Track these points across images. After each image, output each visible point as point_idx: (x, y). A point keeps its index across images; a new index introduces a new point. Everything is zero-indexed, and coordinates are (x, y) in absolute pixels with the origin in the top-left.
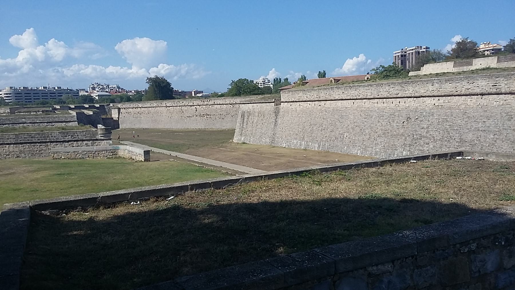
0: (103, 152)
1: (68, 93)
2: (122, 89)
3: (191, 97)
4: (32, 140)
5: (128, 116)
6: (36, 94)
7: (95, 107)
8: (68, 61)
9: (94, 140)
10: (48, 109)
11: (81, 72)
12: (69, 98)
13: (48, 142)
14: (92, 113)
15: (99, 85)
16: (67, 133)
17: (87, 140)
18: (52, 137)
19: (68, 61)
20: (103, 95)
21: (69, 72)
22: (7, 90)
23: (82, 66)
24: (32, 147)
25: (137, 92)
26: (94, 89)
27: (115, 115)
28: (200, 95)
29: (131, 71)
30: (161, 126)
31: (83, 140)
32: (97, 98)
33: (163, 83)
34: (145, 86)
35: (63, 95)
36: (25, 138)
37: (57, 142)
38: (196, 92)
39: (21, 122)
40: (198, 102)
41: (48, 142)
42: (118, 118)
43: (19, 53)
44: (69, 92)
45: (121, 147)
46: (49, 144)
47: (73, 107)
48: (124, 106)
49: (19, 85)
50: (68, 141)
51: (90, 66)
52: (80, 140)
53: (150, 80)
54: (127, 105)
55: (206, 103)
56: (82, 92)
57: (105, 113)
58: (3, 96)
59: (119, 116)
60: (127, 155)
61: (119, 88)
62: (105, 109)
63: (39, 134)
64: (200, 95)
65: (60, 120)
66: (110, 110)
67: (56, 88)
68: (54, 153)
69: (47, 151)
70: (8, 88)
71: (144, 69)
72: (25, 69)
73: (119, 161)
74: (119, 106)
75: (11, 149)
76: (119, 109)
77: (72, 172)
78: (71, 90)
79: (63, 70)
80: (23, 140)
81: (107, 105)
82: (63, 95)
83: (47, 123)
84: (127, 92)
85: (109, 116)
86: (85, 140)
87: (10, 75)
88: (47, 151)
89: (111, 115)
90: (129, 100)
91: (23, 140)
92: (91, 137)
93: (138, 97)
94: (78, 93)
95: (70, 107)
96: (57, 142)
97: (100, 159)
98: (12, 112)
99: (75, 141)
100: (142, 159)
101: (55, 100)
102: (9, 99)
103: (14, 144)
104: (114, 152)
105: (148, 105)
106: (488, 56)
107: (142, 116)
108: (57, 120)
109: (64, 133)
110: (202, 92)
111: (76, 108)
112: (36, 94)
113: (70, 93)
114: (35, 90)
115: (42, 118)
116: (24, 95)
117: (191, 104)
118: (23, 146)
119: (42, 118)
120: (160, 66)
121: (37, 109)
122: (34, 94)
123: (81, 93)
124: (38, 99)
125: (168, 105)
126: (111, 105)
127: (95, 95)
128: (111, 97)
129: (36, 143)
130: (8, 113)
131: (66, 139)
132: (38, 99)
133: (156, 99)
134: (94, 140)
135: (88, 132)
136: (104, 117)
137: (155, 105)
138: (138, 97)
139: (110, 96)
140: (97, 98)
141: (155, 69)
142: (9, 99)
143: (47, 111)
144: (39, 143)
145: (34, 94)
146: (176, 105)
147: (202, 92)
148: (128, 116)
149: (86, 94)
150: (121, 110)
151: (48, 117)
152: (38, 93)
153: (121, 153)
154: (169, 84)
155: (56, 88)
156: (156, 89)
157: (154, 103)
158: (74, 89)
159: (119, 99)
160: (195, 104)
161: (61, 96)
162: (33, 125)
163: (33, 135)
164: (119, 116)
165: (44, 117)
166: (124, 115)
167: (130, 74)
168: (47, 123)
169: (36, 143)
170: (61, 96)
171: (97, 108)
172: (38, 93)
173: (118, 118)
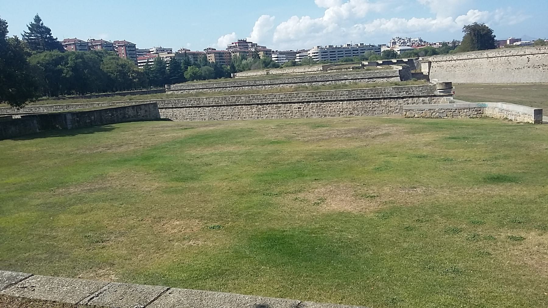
0: (465, 111)
1: (370, 49)
2: (425, 42)
3: (507, 47)
4: (365, 97)
5: (438, 70)
6: (340, 51)
7: (402, 62)
8: (371, 16)
9: (432, 96)
10: (357, 66)
11: (381, 27)
12: (371, 55)
13: (381, 99)
14: (401, 69)
15: (400, 39)
16: (402, 89)
17: (424, 96)
18: (385, 93)
19: (371, 16)
20: (405, 50)
21: (370, 28)
22: (315, 50)
23: (383, 20)
24: (365, 104)
25: (444, 44)
26: (394, 43)
27: (424, 69)
28: (519, 43)
29: (434, 22)
30: (480, 81)
31: (419, 97)
32: (399, 52)
33: (483, 30)
34: (460, 37)
35: (366, 52)
36: (358, 94)
37: (391, 98)
38: (513, 41)
39: (343, 78)
40: (531, 51)
41: (381, 99)
42: (429, 73)
43: (326, 12)
44: (371, 48)
45: (489, 104)
46: (382, 100)
47: (380, 62)
48: (436, 60)
49: (325, 44)
50: (403, 98)
51: (392, 19)
52: (416, 97)
53: (468, 28)
54: (439, 58)
55: (542, 51)
56: (384, 47)
57: (414, 68)
58: (311, 55)
59: (429, 70)
60: (497, 114)
61: (421, 41)
62: (414, 63)
63: (372, 90)
64: (519, 43)
65: (381, 76)
66: (419, 64)
67: (359, 45)
68: (406, 111)
69: (380, 109)
70: (316, 48)
71: (450, 18)
72: (330, 28)
73: (486, 121)
74: (430, 59)
75: (345, 106)
76: (430, 63)
77: (393, 132)
78: (373, 46)
79: (366, 26)
80: (356, 97)
81: (416, 59)
82: (366, 52)
83: (369, 78)
84: (431, 45)
85: (418, 71)
86: (421, 97)
87: (317, 34)
88: (380, 109)
89: (421, 70)
90: (434, 53)
91: (356, 97)
92: (429, 93)
93: (447, 49)
94: (380, 49)
95: (377, 63)
96: (391, 98)
97: (462, 118)
98: (325, 69)
99: (410, 97)
100: (531, 120)
101: (357, 57)
102: (317, 58)
103: (347, 100)
104: (479, 111)
105: (465, 57)
106: (318, 63)
107: (456, 70)
108: (378, 75)
109: (398, 89)
110: (520, 40)
111: (384, 63)
112: (340, 51)
113: (372, 49)
114: (339, 48)
115: (363, 74)
116: (329, 53)
117: (522, 53)
118: (356, 103)
119: (363, 74)
120: (470, 13)
121: (347, 66)
122: (338, 51)
123: (383, 49)
124: (342, 56)
125: (490, 55)
126: (420, 59)
127: (397, 49)
128: (415, 51)
129: (369, 99)
130: (321, 70)
131: (401, 95)
132: (342, 56)
133: (473, 49)
134: (432, 96)
135: (424, 88)
136: (413, 72)
137: (473, 57)
138: (447, 49)
139: (413, 49)
140: (399, 52)
141: (463, 17)
142: (317, 58)
143: (357, 68)
144: (372, 99)
145: (338, 51)
146: (500, 55)
147: (520, 40)
148: (438, 70)
149: (388, 49)
150: (432, 64)
151: (369, 73)
152: (341, 51)
153: (488, 112)
154: (490, 31)
155: (359, 45)
156: (474, 38)
157: (473, 54)
158: (376, 45)
159: (424, 53)
160: (527, 53)
161: (363, 52)
162: (355, 81)
163: (366, 91)
164: (429, 70)
165: (365, 73)
166: (435, 69)
167: (433, 24)
168: (369, 78)
169: (369, 99)
170: (363, 52)
171: (405, 62)
172: (341, 51)
173: (429, 73)
